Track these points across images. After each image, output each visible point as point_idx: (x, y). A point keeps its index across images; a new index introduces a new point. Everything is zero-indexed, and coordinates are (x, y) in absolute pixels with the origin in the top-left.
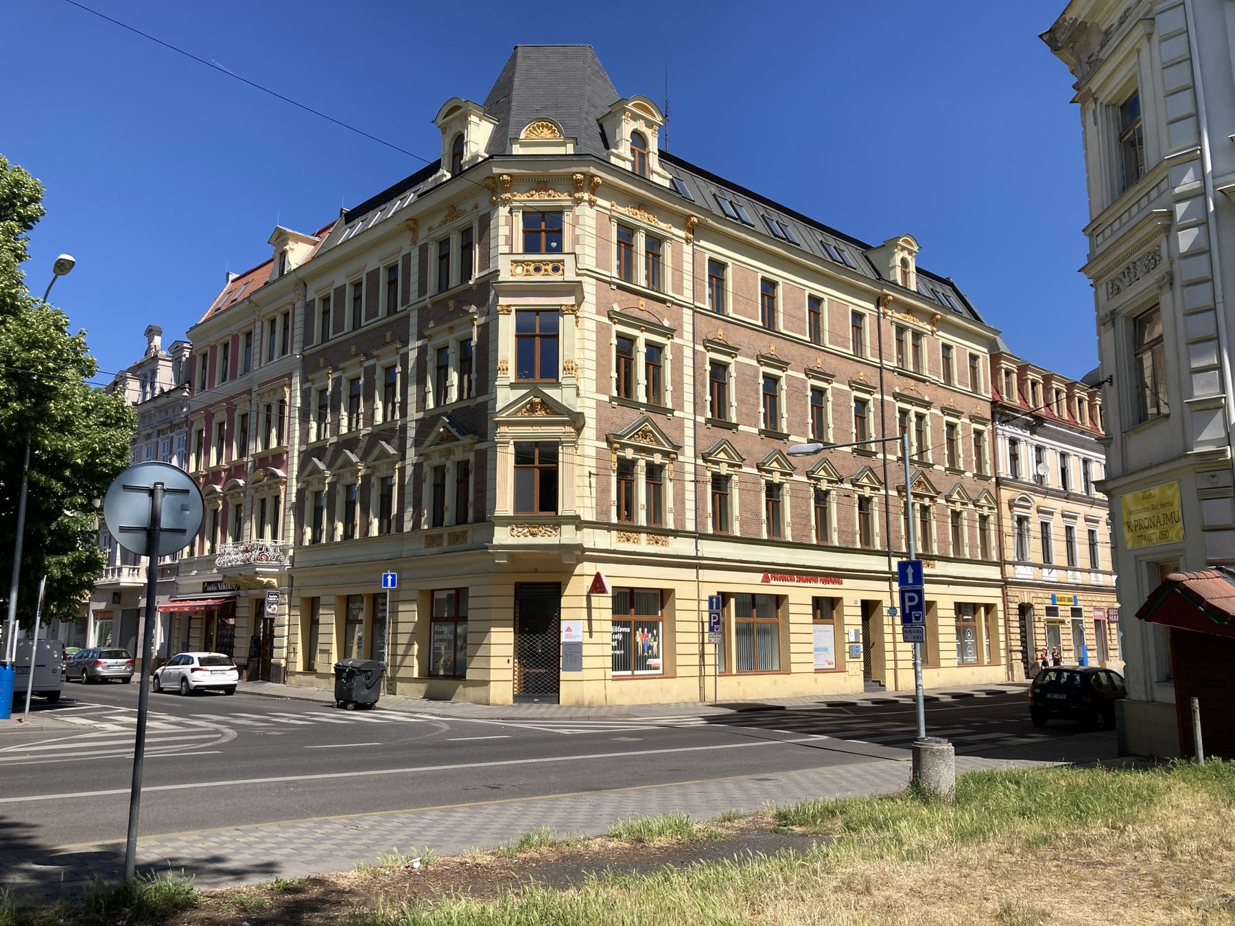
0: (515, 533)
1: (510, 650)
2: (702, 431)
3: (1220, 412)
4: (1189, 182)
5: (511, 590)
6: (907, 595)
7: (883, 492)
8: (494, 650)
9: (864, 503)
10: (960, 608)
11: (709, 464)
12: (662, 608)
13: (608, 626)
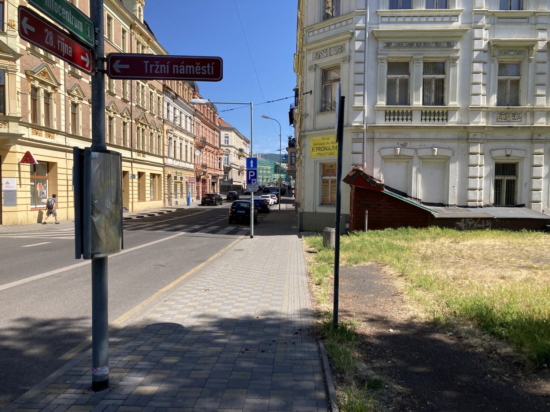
2: (67, 78)
3: (362, 112)
4: (361, 24)
6: (250, 172)
7: (130, 121)
9: (125, 124)
10: (153, 176)
11: (70, 97)
12: (48, 172)
13: (28, 181)
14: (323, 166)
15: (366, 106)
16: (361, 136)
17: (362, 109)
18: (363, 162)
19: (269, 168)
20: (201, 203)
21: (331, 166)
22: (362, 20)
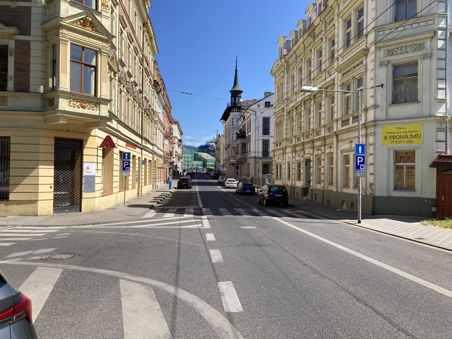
0: (71, 104)
1: (51, 181)
3: (445, 104)
4: (442, 25)
5: (52, 142)
6: (358, 158)
8: (41, 180)
14: (396, 153)
15: (448, 98)
16: (444, 126)
17: (443, 101)
18: (446, 149)
19: (190, 156)
20: (176, 187)
21: (407, 153)
22: (444, 21)
